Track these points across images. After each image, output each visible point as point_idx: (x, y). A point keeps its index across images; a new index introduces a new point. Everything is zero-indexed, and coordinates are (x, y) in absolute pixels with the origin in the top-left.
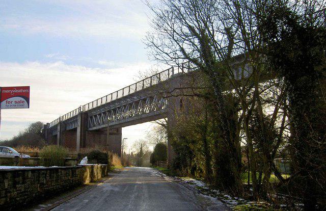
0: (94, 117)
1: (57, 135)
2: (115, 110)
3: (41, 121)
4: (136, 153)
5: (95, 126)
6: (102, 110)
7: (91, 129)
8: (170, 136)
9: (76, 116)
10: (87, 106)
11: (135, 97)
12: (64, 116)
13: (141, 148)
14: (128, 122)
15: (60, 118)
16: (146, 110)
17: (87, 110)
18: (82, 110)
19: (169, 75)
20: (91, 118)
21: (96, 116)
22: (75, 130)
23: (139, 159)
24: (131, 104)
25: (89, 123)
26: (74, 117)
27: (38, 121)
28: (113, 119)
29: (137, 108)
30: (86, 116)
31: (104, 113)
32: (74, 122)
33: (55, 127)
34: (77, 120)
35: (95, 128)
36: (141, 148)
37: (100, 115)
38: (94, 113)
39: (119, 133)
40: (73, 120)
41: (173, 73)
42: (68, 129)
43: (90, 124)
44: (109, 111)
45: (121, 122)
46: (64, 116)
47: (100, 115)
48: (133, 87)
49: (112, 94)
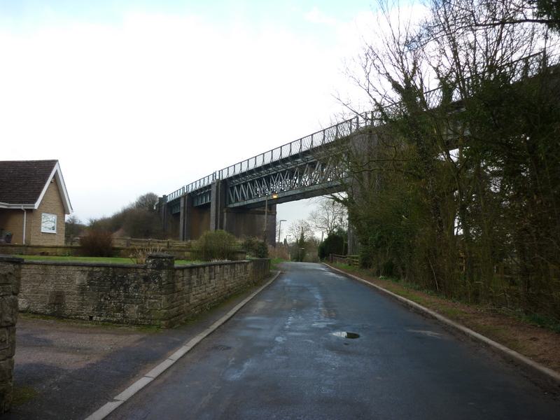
0: (235, 188)
1: (179, 213)
2: (268, 178)
3: (143, 195)
4: (294, 241)
5: (237, 201)
6: (242, 180)
7: (231, 206)
8: (353, 218)
9: (209, 186)
10: (238, 167)
11: (299, 160)
12: (190, 186)
13: (302, 234)
14: (289, 196)
15: (183, 188)
16: (306, 180)
17: (225, 176)
18: (217, 177)
19: (351, 128)
20: (232, 189)
21: (239, 187)
22: (208, 206)
23: (302, 249)
24: (283, 173)
25: (228, 195)
26: (205, 188)
27: (144, 193)
28: (261, 193)
29: (291, 178)
30: (226, 186)
31: (252, 182)
32: (206, 194)
33: (177, 201)
34: (210, 192)
35: (237, 205)
36: (302, 234)
37: (245, 184)
38: (236, 182)
39: (273, 213)
40: (205, 191)
41: (358, 126)
42: (196, 205)
43: (230, 198)
44: (260, 180)
45: (286, 194)
46: (190, 186)
47: (245, 184)
48: (231, 171)
49: (264, 154)
